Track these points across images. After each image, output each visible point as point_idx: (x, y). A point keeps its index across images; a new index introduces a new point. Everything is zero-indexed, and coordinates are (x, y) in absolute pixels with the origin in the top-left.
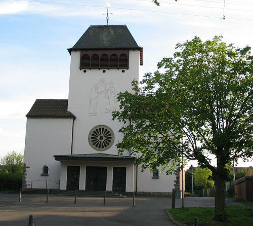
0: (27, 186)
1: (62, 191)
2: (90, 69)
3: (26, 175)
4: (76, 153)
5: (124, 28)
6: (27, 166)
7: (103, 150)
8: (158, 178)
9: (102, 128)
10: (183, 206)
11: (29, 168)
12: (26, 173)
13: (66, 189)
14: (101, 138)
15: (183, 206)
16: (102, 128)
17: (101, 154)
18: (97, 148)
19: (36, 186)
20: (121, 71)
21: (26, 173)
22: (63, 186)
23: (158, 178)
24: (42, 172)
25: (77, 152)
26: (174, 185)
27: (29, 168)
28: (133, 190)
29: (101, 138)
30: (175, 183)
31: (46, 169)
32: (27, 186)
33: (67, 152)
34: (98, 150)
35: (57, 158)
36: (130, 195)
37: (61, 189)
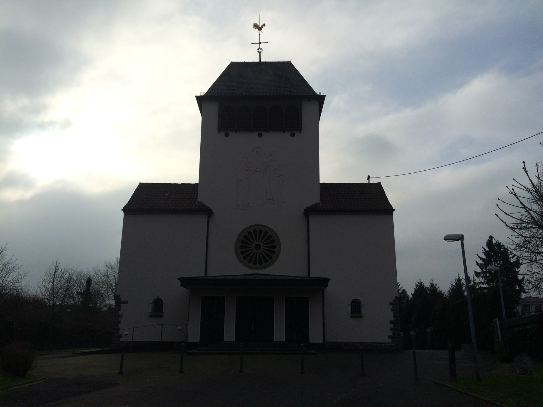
0: (121, 337)
1: (193, 345)
2: (236, 131)
3: (121, 316)
4: (213, 272)
5: (288, 66)
6: (122, 300)
7: (265, 268)
8: (361, 317)
9: (258, 230)
10: (161, 340)
11: (126, 302)
12: (120, 313)
13: (234, 340)
14: (258, 247)
15: (161, 340)
16: (258, 230)
17: (258, 274)
18: (251, 264)
19: (142, 336)
20: (255, 134)
21: (120, 313)
22: (194, 336)
23: (361, 317)
24: (150, 309)
25: (215, 271)
26: (391, 329)
27: (126, 302)
28: (320, 341)
29: (258, 247)
30: (392, 326)
31: (158, 305)
32: (121, 337)
33: (199, 273)
34: (251, 268)
35: (185, 282)
36: (316, 346)
37: (189, 341)
